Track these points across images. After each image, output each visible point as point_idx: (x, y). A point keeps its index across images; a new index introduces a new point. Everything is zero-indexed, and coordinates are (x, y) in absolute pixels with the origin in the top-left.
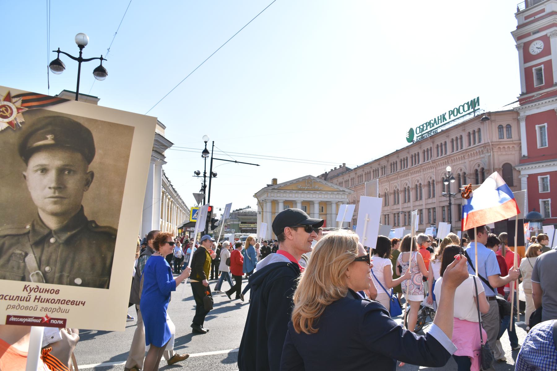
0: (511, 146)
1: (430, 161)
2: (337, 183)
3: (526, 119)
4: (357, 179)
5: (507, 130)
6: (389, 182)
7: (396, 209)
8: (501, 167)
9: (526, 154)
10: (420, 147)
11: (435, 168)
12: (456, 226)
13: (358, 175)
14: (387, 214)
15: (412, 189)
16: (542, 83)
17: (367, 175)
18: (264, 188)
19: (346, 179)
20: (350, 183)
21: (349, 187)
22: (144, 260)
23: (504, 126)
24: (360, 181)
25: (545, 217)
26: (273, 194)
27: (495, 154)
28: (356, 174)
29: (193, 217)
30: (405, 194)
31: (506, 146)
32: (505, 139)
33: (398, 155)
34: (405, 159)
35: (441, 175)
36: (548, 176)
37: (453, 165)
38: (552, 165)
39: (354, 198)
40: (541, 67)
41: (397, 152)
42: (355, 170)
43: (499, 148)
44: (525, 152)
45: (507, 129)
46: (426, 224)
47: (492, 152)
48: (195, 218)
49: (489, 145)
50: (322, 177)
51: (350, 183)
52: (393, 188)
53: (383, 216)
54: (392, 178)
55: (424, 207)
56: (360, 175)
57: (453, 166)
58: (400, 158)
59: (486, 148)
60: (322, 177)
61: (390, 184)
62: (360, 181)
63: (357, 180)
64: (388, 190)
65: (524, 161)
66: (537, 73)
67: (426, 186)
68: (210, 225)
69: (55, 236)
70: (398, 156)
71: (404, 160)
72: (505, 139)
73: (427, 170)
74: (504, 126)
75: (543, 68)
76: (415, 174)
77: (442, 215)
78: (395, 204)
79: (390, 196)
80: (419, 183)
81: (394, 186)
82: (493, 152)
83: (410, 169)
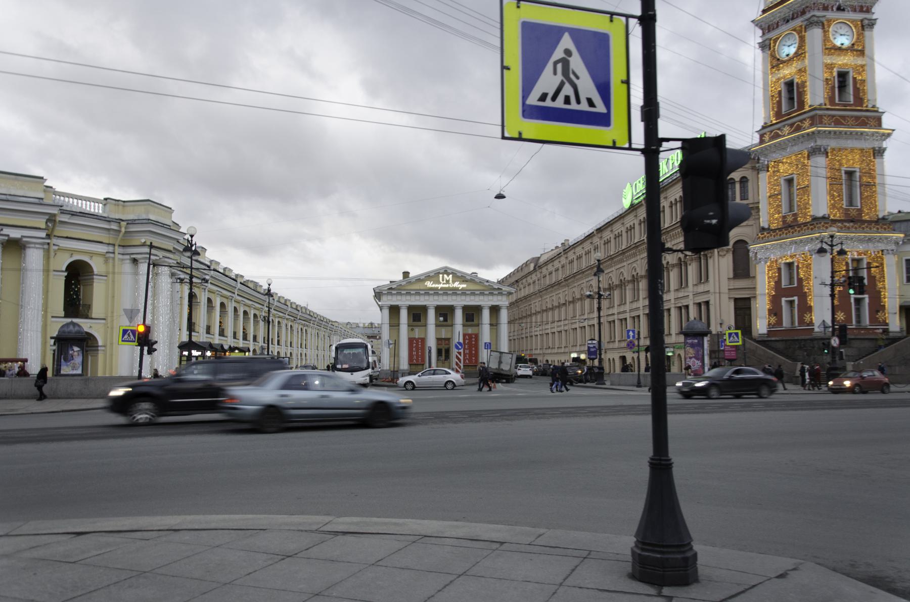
2: (611, 236)
4: (603, 246)
5: (742, 186)
7: (702, 293)
13: (640, 220)
14: (684, 306)
16: (794, 108)
17: (674, 207)
19: (587, 250)
28: (567, 258)
29: (533, 100)
30: (681, 268)
33: (636, 213)
42: (565, 252)
45: (742, 185)
48: (548, 103)
52: (619, 277)
53: (676, 309)
56: (676, 199)
58: (639, 218)
63: (568, 267)
64: (614, 280)
66: (788, 89)
67: (694, 261)
68: (146, 348)
70: (635, 215)
73: (674, 238)
78: (700, 282)
79: (569, 305)
81: (619, 273)
83: (624, 251)
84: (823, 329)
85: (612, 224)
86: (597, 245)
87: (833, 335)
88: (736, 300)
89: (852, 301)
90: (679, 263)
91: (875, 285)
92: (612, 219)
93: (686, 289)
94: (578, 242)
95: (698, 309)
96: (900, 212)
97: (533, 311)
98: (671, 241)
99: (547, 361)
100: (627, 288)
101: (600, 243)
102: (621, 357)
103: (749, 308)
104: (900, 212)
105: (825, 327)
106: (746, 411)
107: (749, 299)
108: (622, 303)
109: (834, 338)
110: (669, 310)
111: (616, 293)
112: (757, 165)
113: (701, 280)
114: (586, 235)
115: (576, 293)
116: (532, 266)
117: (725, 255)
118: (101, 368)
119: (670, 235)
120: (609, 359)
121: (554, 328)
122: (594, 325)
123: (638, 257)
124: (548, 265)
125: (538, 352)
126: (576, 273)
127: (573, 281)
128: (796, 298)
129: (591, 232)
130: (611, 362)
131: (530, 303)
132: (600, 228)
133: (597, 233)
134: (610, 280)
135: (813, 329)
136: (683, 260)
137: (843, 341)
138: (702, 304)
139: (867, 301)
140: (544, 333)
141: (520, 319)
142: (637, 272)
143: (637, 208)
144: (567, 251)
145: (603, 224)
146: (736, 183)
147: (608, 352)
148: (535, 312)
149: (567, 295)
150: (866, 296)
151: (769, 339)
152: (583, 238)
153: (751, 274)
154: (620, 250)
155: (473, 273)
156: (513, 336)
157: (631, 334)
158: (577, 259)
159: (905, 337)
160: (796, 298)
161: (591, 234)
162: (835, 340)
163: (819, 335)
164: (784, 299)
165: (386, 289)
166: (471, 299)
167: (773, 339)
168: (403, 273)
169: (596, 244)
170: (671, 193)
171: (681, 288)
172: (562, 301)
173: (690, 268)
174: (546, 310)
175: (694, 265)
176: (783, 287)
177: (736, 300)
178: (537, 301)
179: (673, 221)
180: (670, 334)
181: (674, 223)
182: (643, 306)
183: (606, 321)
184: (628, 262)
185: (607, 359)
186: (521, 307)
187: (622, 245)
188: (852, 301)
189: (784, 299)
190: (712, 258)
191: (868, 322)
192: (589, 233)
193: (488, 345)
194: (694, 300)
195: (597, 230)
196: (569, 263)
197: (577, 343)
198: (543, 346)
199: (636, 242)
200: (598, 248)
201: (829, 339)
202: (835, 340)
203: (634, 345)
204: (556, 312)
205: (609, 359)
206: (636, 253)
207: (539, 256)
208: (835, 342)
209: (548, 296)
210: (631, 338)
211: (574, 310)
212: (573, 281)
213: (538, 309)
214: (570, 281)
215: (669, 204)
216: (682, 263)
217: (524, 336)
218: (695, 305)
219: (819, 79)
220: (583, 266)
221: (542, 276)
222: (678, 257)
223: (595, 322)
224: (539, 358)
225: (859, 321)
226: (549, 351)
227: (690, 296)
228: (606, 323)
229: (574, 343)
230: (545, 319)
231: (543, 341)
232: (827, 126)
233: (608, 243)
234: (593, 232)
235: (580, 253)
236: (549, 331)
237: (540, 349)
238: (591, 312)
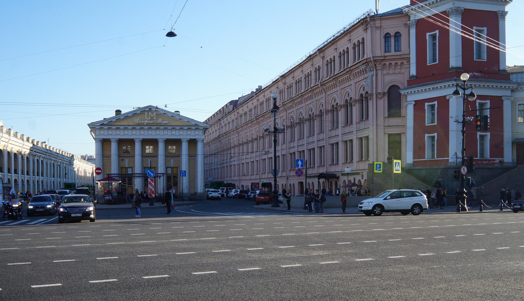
0: (399, 62)
1: (319, 83)
3: (416, 25)
6: (286, 111)
7: (292, 147)
8: (386, 91)
9: (415, 74)
10: (312, 63)
11: (325, 92)
12: (358, 169)
13: (340, 52)
14: (312, 149)
15: (356, 101)
17: (346, 55)
18: (91, 123)
20: (303, 84)
21: (264, 112)
22: (496, 68)
23: (392, 34)
24: (262, 111)
25: (490, 158)
26: (190, 131)
27: (379, 72)
31: (393, 63)
32: (393, 53)
34: (345, 51)
35: (290, 119)
36: (436, 103)
37: (356, 82)
38: (439, 88)
39: (310, 110)
40: (436, 34)
41: (283, 77)
43: (385, 64)
44: (413, 71)
45: (396, 39)
46: (342, 163)
47: (375, 71)
49: (371, 61)
50: (230, 105)
51: (303, 84)
54: (357, 71)
55: (340, 139)
57: (356, 83)
59: (368, 65)
60: (230, 105)
61: (287, 114)
62: (262, 111)
64: (314, 111)
65: (414, 82)
69: (134, 192)
70: (349, 38)
71: (331, 63)
72: (393, 53)
74: (392, 34)
75: (438, 35)
76: (361, 75)
77: (337, 154)
79: (260, 140)
80: (365, 91)
82: (376, 70)
84: (455, 160)
85: (293, 71)
86: (282, 89)
87: (463, 165)
88: (390, 135)
89: (478, 137)
90: (346, 104)
91: (106, 192)
92: (286, 72)
93: (366, 122)
94: (267, 87)
95: (360, 142)
96: (515, 66)
97: (232, 145)
98: (340, 86)
99: (243, 186)
100: (305, 125)
101: (284, 88)
102: (299, 182)
103: (400, 143)
104: (515, 66)
105: (457, 158)
106: (143, 187)
107: (399, 135)
108: (311, 134)
109: (463, 167)
110: (279, 156)
111: (306, 126)
112: (408, 22)
113: (363, 118)
114: (273, 81)
115: (304, 114)
116: (232, 107)
117: (381, 98)
118: (441, 180)
119: (326, 87)
120: (290, 184)
121: (303, 145)
122: (272, 158)
123: (338, 88)
124: (249, 104)
125: (235, 178)
126: (265, 112)
127: (263, 120)
128: (435, 134)
129: (277, 78)
130: (292, 187)
131: (230, 138)
132: (285, 74)
133: (319, 53)
134: (301, 115)
135: (449, 159)
136: (349, 102)
137: (470, 171)
138: (363, 139)
139: (489, 137)
140: (240, 163)
141: (222, 151)
142: (313, 112)
143: (351, 31)
144: (258, 94)
145: (286, 72)
146: (392, 37)
147: (289, 179)
148: (233, 146)
149: (258, 131)
150: (488, 134)
151: (414, 168)
152: (271, 83)
153: (402, 115)
154: (300, 93)
155: (176, 112)
156: (206, 168)
157: (300, 163)
158: (266, 101)
159: (515, 167)
160: (435, 134)
161: (277, 80)
162: (464, 169)
163: (453, 165)
164: (426, 135)
165: (99, 124)
166: (180, 133)
167: (417, 168)
168: (116, 111)
169: (281, 89)
170: (328, 53)
171: (347, 125)
172: (254, 137)
173: (354, 108)
174: (242, 144)
175: (343, 111)
176: (426, 125)
177: (390, 135)
178: (235, 136)
179: (356, 61)
180: (315, 167)
181: (356, 62)
182: (317, 141)
183: (288, 153)
184: (356, 81)
185: (289, 185)
186: (223, 141)
187: (311, 84)
188: (478, 137)
189: (426, 135)
190: (371, 100)
191: (489, 156)
192: (276, 79)
193: (183, 172)
194: (357, 136)
195: (319, 50)
196: (260, 105)
197: (235, 175)
198: (239, 174)
199: (350, 66)
200: (282, 92)
201: (460, 168)
202: (464, 169)
203: (302, 173)
204: (250, 145)
205: (290, 184)
206: (312, 96)
207: (238, 99)
208: (464, 170)
209: (243, 133)
210: (300, 167)
211: (264, 143)
212: (263, 120)
213: (236, 143)
214: (260, 120)
215: (338, 55)
216: (364, 99)
217: (225, 165)
218: (358, 140)
219: (264, 94)
220: (259, 113)
221: (239, 116)
222: (360, 94)
223: (272, 155)
224: (237, 184)
225: (482, 154)
226: (244, 178)
227: (339, 135)
228: (288, 154)
229: (263, 171)
230: (245, 151)
231: (239, 169)
232: (33, 250)
233: (290, 87)
234: (279, 79)
235: (291, 82)
236: (244, 161)
237: (237, 176)
238: (270, 147)
